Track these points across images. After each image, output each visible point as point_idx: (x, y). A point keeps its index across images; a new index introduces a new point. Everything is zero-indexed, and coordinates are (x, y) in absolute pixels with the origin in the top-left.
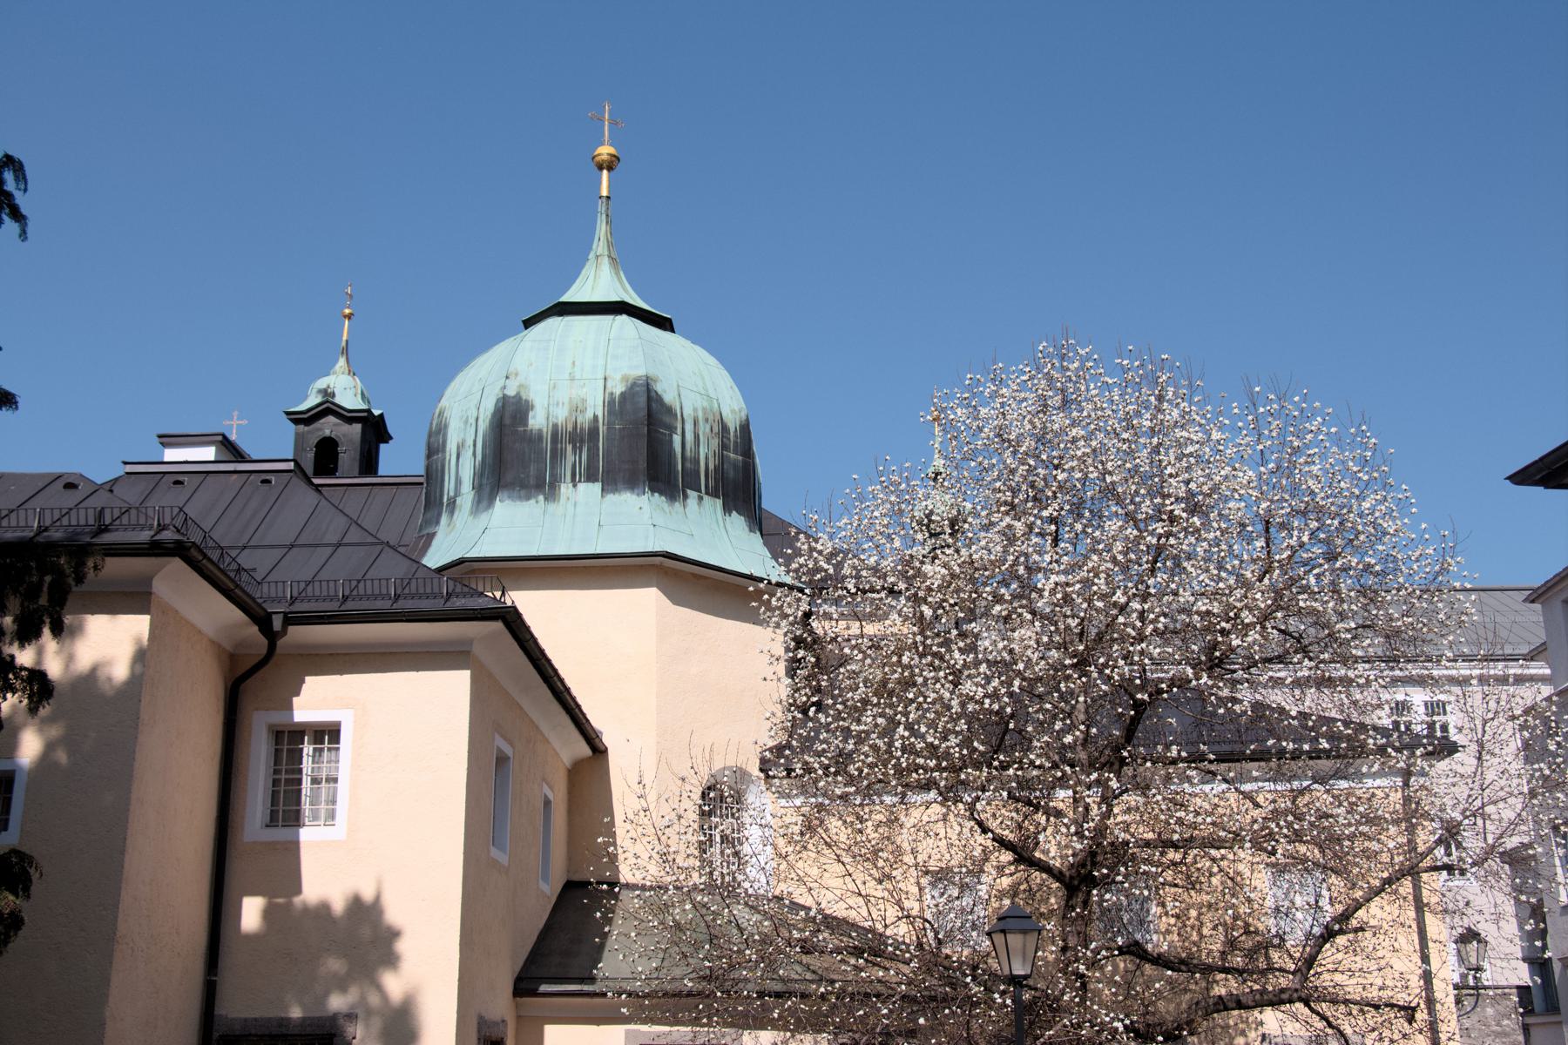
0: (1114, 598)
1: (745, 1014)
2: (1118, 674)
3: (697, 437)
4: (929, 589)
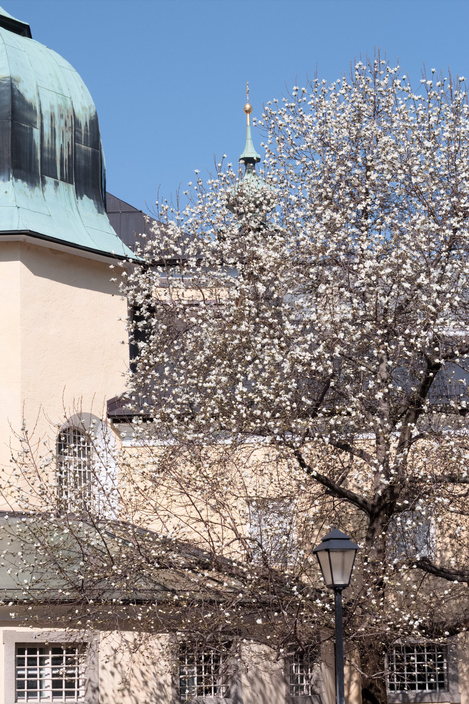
0: (419, 281)
1: (112, 618)
2: (421, 343)
3: (53, 131)
4: (262, 269)
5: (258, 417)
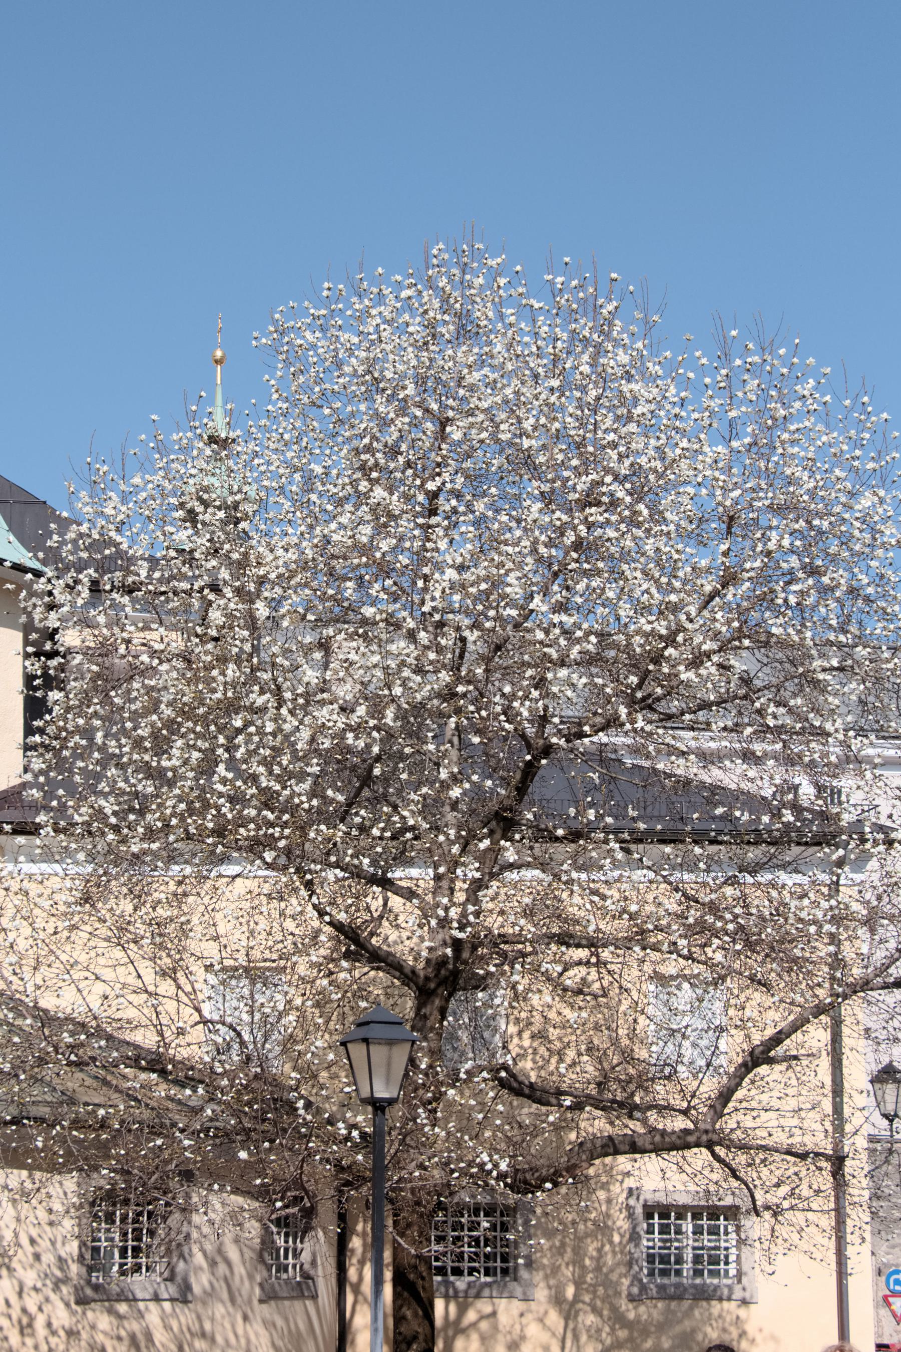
5: (252, 820)
